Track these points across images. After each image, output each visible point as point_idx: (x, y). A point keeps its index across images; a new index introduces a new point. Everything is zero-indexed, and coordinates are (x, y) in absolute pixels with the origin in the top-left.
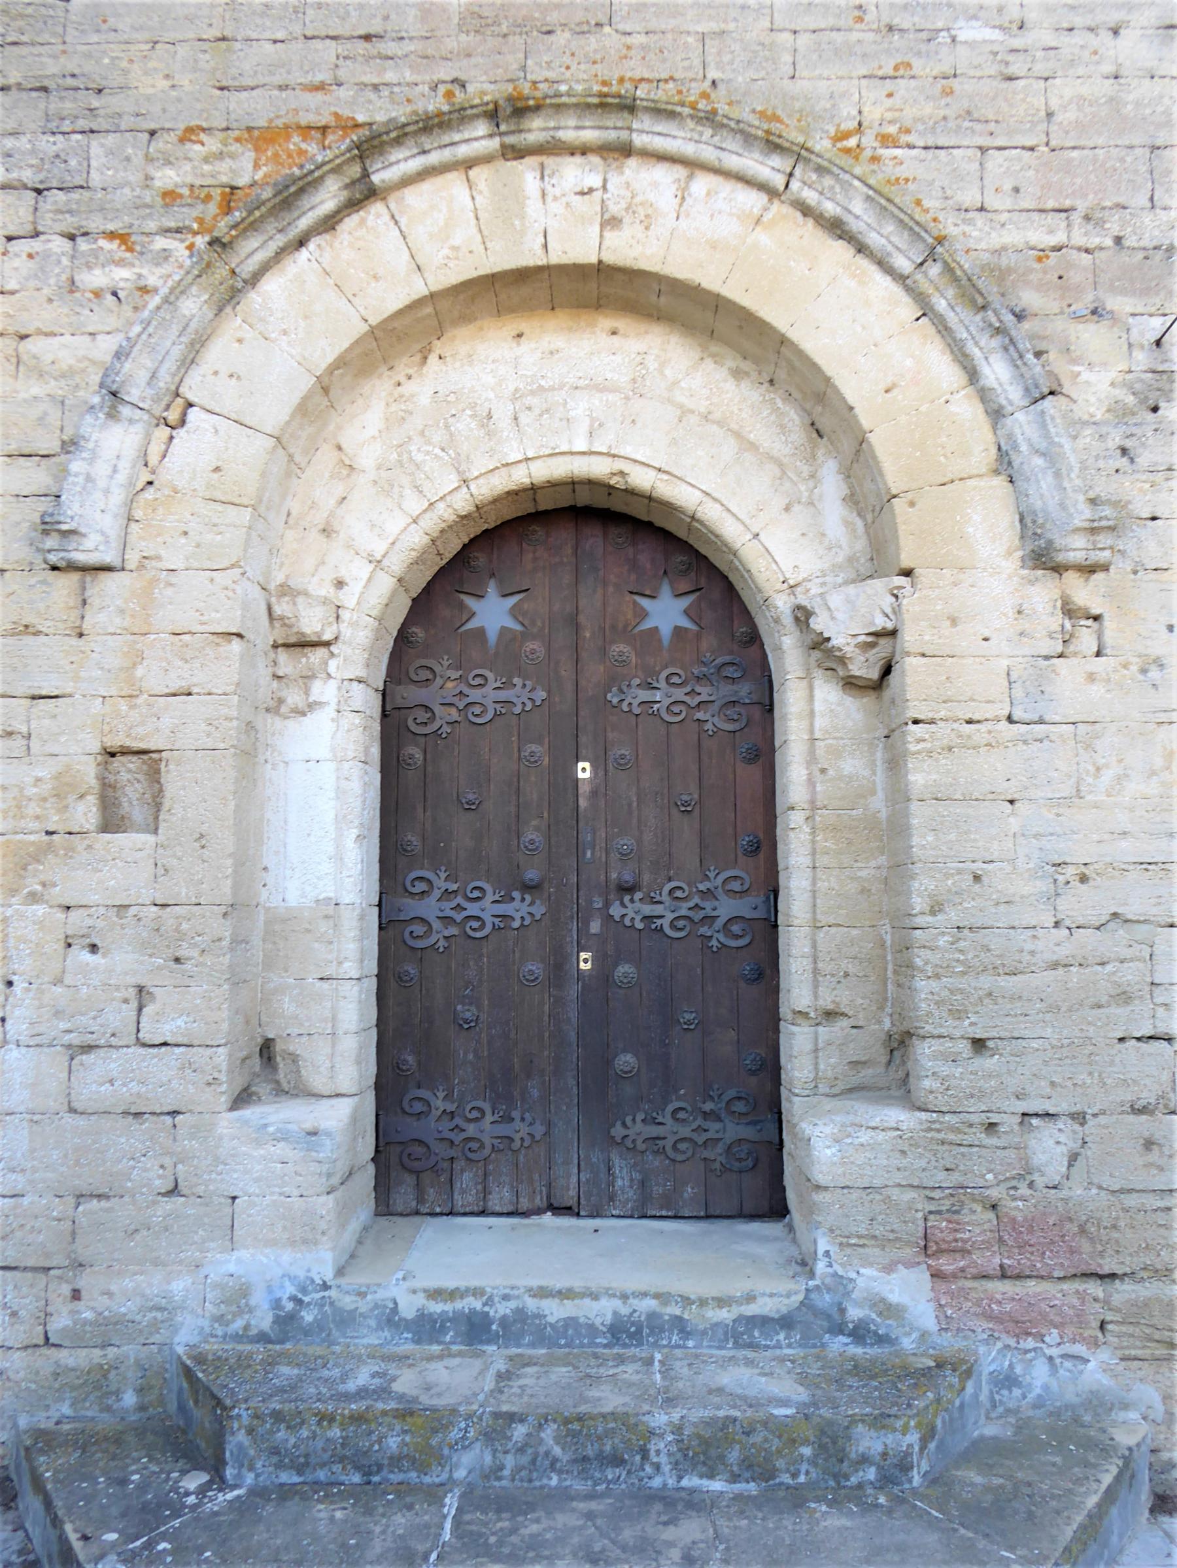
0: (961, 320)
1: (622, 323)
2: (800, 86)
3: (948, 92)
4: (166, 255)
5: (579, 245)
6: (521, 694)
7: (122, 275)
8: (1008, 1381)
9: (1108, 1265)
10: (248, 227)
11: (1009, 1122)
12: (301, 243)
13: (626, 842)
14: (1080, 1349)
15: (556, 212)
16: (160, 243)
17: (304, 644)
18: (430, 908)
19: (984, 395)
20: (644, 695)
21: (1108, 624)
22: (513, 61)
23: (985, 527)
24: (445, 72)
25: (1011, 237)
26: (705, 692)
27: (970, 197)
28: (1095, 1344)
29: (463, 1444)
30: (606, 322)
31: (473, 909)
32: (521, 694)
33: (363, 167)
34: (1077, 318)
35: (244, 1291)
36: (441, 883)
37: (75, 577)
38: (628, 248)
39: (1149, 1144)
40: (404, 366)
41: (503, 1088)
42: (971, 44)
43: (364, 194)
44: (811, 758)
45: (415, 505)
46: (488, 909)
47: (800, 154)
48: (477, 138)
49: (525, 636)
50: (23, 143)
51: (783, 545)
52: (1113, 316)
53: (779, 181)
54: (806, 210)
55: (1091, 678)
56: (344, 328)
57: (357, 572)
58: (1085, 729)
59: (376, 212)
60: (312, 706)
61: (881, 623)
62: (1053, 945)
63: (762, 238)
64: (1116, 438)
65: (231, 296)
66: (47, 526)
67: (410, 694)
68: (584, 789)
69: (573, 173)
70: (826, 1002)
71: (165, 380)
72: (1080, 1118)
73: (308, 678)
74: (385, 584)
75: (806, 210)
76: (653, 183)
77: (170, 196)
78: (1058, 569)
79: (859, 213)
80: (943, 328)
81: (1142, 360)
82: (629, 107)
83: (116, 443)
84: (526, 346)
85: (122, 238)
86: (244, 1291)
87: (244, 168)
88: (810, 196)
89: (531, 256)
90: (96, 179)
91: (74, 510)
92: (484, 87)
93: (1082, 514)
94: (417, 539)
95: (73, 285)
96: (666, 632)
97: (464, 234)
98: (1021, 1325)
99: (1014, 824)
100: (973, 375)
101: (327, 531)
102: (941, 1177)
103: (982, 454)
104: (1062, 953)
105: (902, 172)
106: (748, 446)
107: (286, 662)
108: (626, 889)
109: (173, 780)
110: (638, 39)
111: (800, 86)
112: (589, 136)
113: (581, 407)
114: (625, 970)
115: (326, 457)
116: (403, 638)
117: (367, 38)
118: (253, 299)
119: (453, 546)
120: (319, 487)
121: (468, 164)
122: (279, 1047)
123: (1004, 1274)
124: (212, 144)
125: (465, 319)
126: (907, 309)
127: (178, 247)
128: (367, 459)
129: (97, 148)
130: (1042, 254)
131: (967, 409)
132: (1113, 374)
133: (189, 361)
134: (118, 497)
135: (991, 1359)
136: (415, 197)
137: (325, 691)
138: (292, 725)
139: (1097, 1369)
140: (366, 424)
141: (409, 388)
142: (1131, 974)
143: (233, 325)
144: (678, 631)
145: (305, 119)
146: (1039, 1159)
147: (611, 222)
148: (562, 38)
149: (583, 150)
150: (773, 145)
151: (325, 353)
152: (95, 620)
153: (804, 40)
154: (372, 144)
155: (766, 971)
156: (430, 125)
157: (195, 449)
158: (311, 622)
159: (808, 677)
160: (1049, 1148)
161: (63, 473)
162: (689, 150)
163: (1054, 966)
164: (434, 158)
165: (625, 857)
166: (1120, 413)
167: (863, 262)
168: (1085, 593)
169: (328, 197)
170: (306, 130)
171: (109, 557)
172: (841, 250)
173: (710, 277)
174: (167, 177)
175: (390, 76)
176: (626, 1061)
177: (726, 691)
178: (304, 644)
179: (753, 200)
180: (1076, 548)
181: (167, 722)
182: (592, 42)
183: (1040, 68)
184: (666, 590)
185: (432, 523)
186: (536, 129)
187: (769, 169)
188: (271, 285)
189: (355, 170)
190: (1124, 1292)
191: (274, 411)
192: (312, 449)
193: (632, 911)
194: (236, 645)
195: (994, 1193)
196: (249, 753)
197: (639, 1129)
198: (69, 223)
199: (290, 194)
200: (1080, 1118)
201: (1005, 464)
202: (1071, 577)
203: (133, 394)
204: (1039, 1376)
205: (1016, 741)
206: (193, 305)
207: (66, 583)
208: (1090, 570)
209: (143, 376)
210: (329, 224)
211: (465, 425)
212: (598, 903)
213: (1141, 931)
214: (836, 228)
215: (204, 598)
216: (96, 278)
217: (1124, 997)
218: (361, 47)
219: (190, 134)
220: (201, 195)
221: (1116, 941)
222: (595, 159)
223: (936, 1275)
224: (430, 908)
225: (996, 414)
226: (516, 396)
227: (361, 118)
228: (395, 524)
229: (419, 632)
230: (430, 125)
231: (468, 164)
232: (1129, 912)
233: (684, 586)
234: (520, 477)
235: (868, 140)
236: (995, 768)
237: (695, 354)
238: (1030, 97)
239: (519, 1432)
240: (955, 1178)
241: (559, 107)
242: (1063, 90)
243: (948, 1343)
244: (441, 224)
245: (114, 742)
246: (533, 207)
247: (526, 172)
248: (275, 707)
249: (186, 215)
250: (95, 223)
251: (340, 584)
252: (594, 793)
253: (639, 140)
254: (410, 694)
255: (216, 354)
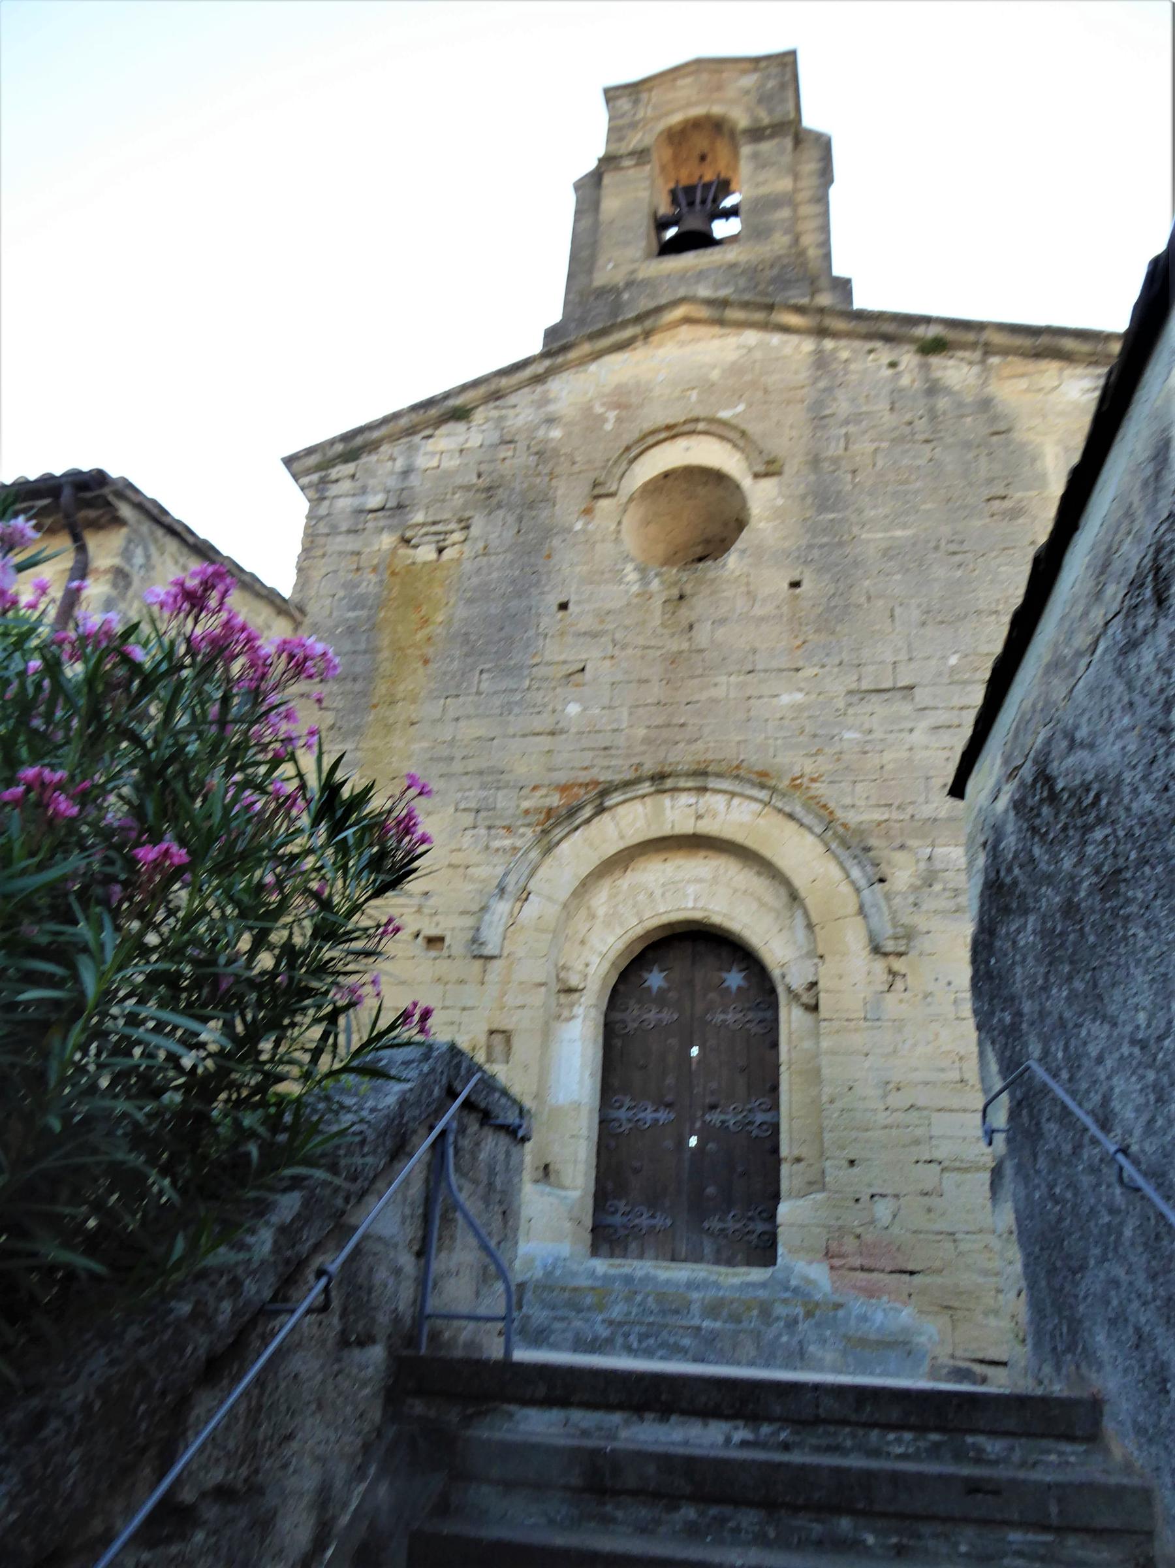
0: (840, 851)
1: (710, 853)
2: (777, 760)
3: (838, 760)
4: (523, 835)
5: (687, 826)
6: (668, 1016)
7: (507, 843)
8: (864, 1318)
9: (910, 1267)
10: (556, 825)
11: (865, 1198)
12: (577, 828)
13: (714, 1085)
14: (898, 1305)
15: (677, 813)
16: (522, 830)
17: (570, 991)
18: (622, 1114)
19: (853, 883)
20: (722, 1017)
21: (909, 978)
22: (661, 755)
23: (854, 938)
24: (635, 760)
25: (866, 817)
26: (750, 1015)
27: (848, 801)
28: (905, 1304)
29: (615, 1302)
30: (702, 854)
31: (641, 1115)
32: (668, 1016)
33: (602, 797)
34: (894, 849)
35: (533, 1260)
36: (628, 1103)
37: (481, 962)
38: (706, 827)
39: (929, 1210)
40: (617, 874)
41: (653, 1202)
42: (850, 740)
43: (601, 810)
44: (790, 1042)
45: (620, 932)
46: (649, 1115)
47: (774, 790)
48: (646, 788)
49: (669, 990)
50: (472, 793)
51: (777, 948)
52: (910, 849)
53: (767, 799)
54: (780, 811)
55: (901, 1001)
56: (593, 860)
57: (595, 960)
58: (899, 1024)
59: (606, 816)
60: (572, 1018)
61: (811, 979)
62: (882, 1118)
63: (761, 821)
64: (911, 899)
65: (548, 850)
66: (474, 940)
67: (618, 1016)
68: (694, 1061)
69: (685, 799)
70: (796, 1153)
71: (521, 884)
72: (896, 1196)
73: (572, 1005)
74: (606, 965)
75: (780, 811)
76: (717, 802)
77: (527, 812)
78: (886, 955)
79: (798, 810)
80: (836, 857)
81: (923, 865)
82: (704, 774)
83: (502, 908)
84: (668, 864)
85: (508, 828)
86: (533, 1260)
87: (555, 800)
88: (779, 805)
89: (666, 831)
90: (499, 806)
91: (485, 934)
92: (649, 767)
93: (890, 931)
94: (620, 946)
95: (487, 847)
96: (734, 987)
97: (641, 823)
98: (871, 1293)
99: (867, 1065)
100: (848, 876)
101: (583, 942)
102: (833, 1222)
103: (853, 907)
104: (889, 1121)
105: (819, 793)
106: (762, 904)
107: (563, 998)
108: (713, 1107)
109: (516, 1042)
110: (712, 745)
111: (777, 760)
112: (690, 784)
113: (691, 889)
114: (711, 1146)
115: (583, 913)
116: (615, 990)
117: (606, 749)
118: (557, 851)
119: (638, 950)
120: (580, 924)
121: (644, 796)
122: (551, 1167)
123: (863, 1269)
124: (543, 791)
125: (641, 854)
126: (821, 849)
127: (529, 832)
128: (601, 912)
129: (500, 794)
130: (879, 824)
131: (845, 889)
132: (909, 872)
133: (531, 875)
134: (501, 929)
135: (858, 1306)
136: (621, 810)
137: (579, 1011)
138: (564, 1026)
139: (906, 1315)
140: (601, 899)
141: (619, 882)
142: (919, 1132)
143: (549, 861)
144: (739, 988)
145: (580, 780)
146: (878, 1215)
147: (699, 817)
148: (681, 745)
149: (689, 789)
150: (763, 786)
151: (584, 872)
152: (490, 977)
153: (779, 742)
154: (604, 793)
155: (776, 1150)
156: (627, 784)
157: (531, 909)
158: (574, 981)
159: (788, 1004)
160: (883, 1210)
161: (480, 920)
162: (730, 788)
163: (886, 1127)
164: (628, 796)
165: (712, 1093)
166: (915, 889)
167: (802, 831)
168: (898, 965)
169: (587, 812)
170: (581, 785)
171: (496, 952)
172: (792, 826)
173: (739, 837)
174: (526, 804)
175: (613, 763)
176: (711, 1190)
177: (761, 1015)
178: (570, 991)
179: (756, 807)
180: (889, 946)
181: (514, 1019)
182: (693, 747)
183: (879, 748)
184: (735, 969)
185: (627, 939)
186: (669, 783)
187: (763, 795)
188: (564, 845)
189: (598, 802)
190: (917, 1279)
191: (564, 894)
192: (578, 908)
193: (715, 1118)
194: (543, 989)
195: (858, 1231)
196: (547, 1035)
197: (714, 1224)
198: (488, 823)
199: (573, 812)
200: (896, 1196)
201: (861, 910)
202: (891, 958)
203: (510, 889)
204: (879, 1317)
205: (868, 1028)
206: (534, 855)
207: (478, 964)
208: (900, 955)
209: (513, 882)
210: (588, 821)
211: (641, 897)
212: (699, 1113)
213: (925, 1113)
214: (791, 816)
215: (534, 970)
216: (496, 844)
217: (917, 1142)
218: (602, 753)
219: (535, 788)
220: (538, 811)
221: (913, 1116)
222: (693, 793)
223: (832, 1268)
224: (622, 1114)
225: (858, 891)
226: (663, 885)
227: (602, 779)
228: (611, 940)
229: (622, 988)
230: (627, 784)
231: (644, 796)
232: (920, 1104)
233: (743, 966)
234: (665, 919)
235: (805, 780)
236: (858, 1040)
237: (740, 866)
238: (873, 760)
239: (639, 1298)
240: (840, 1223)
241: (678, 776)
242: (887, 756)
243: (837, 1298)
244: (631, 820)
245: (495, 1027)
246: (668, 812)
247: (666, 800)
248: (558, 1017)
249: (533, 819)
250: (498, 823)
251: (587, 965)
252: (699, 1062)
253: (711, 786)
254: (618, 1016)
255: (542, 872)
